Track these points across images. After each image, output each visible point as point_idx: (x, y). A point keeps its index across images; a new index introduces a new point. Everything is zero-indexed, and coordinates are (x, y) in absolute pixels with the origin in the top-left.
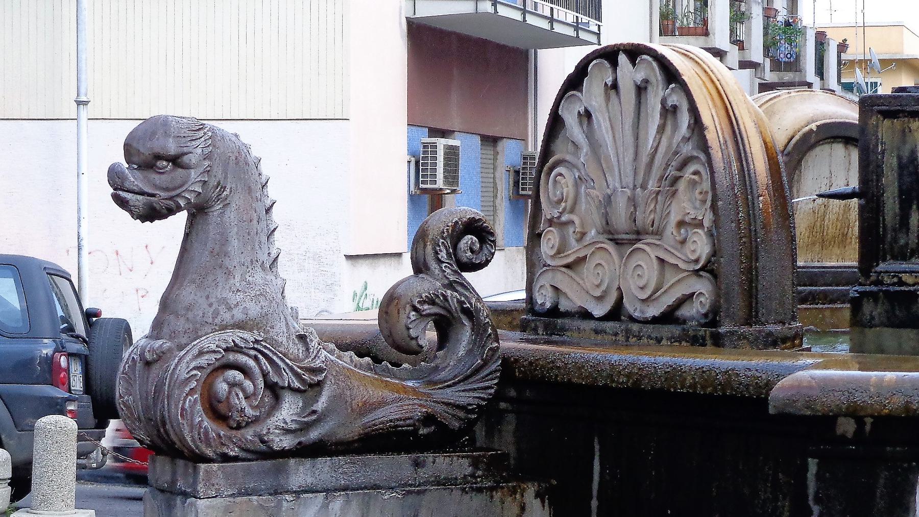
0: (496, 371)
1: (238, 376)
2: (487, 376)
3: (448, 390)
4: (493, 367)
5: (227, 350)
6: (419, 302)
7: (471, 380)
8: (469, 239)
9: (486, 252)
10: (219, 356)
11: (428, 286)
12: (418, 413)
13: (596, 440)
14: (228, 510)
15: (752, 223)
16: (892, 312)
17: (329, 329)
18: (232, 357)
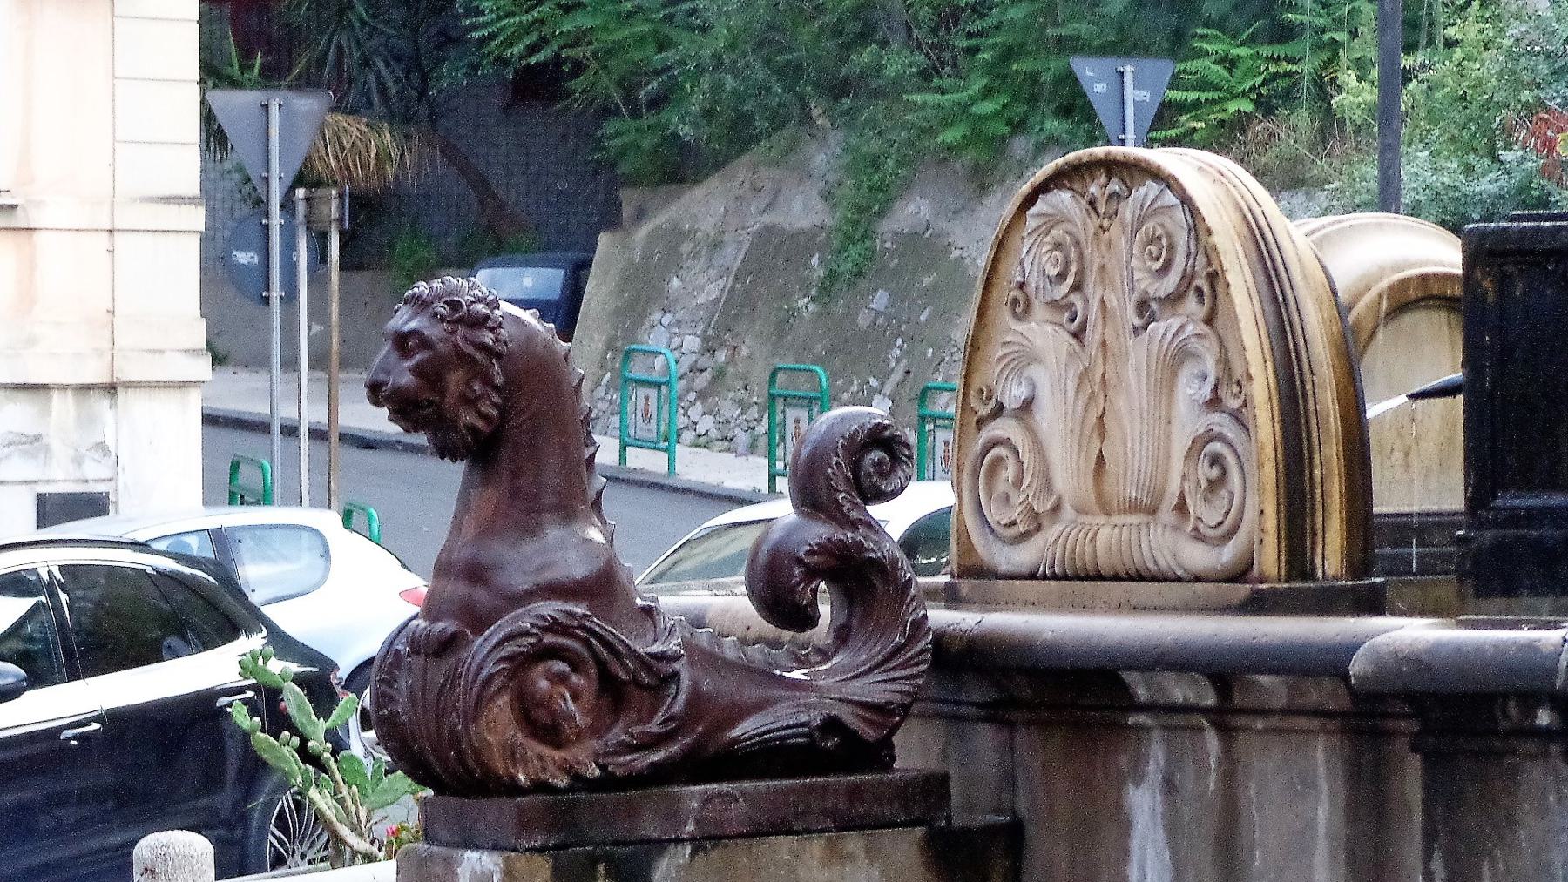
0: (923, 651)
1: (561, 666)
2: (911, 658)
3: (856, 683)
4: (922, 644)
5: (544, 629)
6: (807, 553)
7: (890, 665)
8: (876, 455)
9: (900, 474)
10: (533, 640)
11: (820, 531)
12: (816, 718)
13: (737, 732)
14: (689, 868)
15: (1316, 441)
16: (1495, 560)
17: (1048, 635)
18: (548, 639)
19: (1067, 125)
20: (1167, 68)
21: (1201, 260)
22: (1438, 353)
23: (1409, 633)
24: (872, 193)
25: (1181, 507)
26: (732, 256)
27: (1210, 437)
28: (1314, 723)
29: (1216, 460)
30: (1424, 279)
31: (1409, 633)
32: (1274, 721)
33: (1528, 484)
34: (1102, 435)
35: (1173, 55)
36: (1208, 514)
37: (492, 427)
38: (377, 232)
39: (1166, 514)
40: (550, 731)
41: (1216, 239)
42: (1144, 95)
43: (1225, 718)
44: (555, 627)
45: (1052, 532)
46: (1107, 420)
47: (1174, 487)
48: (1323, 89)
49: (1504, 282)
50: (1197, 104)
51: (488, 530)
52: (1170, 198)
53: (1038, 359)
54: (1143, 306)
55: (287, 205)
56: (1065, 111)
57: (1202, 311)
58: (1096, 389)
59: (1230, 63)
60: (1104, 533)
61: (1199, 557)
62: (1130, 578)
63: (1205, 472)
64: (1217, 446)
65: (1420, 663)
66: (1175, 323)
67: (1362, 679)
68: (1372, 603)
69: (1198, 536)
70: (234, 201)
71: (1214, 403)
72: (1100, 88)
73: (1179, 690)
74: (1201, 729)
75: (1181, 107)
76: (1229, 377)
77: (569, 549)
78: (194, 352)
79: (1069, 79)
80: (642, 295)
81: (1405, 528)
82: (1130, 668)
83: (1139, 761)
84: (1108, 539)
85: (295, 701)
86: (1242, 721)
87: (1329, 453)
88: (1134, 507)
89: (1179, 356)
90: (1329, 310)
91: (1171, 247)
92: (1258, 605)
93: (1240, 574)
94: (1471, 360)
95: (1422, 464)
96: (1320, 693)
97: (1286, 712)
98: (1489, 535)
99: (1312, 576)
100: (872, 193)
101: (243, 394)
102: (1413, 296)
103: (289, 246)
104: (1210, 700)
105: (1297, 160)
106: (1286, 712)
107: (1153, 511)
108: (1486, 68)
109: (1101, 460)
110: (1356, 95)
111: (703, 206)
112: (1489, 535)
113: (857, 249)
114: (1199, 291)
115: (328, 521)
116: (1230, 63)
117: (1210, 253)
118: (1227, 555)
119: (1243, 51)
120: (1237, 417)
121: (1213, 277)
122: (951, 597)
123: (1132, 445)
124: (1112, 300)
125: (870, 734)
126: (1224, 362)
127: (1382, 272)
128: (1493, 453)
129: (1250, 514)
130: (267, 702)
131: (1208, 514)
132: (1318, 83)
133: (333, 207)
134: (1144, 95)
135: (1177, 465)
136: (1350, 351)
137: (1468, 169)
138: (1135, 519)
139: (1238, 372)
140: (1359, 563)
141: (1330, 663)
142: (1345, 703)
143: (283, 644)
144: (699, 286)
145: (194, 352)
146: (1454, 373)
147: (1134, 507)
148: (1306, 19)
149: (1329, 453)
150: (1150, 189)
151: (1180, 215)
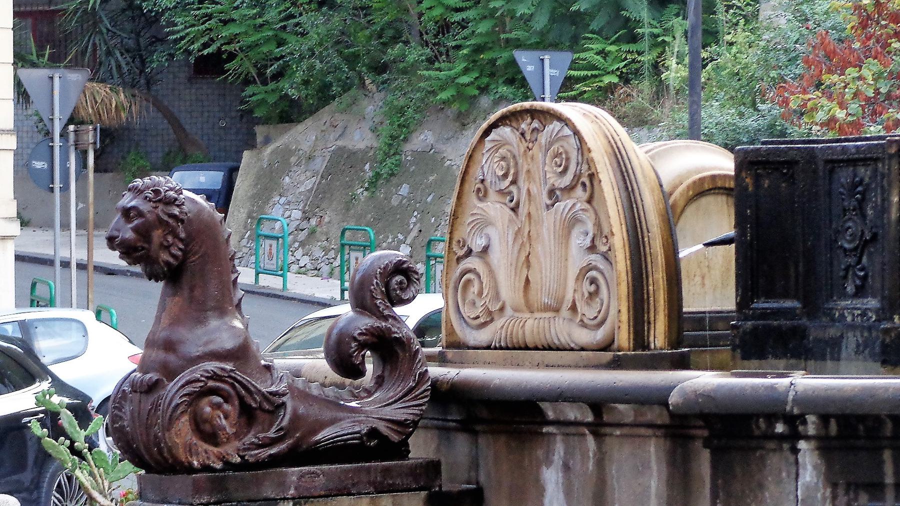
15: (650, 271)
20: (567, 57)
21: (585, 167)
22: (719, 218)
23: (703, 380)
24: (400, 129)
25: (574, 308)
26: (320, 164)
27: (590, 268)
28: (650, 432)
29: (593, 281)
30: (713, 177)
31: (703, 380)
32: (626, 430)
33: (770, 295)
34: (528, 267)
36: (589, 312)
37: (177, 261)
38: (114, 150)
39: (565, 312)
40: (212, 437)
42: (555, 72)
44: (215, 377)
45: (499, 323)
47: (569, 297)
48: (657, 68)
49: (757, 179)
50: (585, 78)
51: (175, 322)
53: (492, 223)
54: (552, 193)
55: (64, 135)
56: (510, 82)
58: (524, 241)
59: (603, 53)
60: (530, 323)
61: (584, 337)
64: (593, 273)
65: (708, 396)
66: (570, 203)
67: (676, 406)
68: (682, 363)
69: (583, 325)
70: (34, 134)
71: (592, 248)
72: (530, 68)
73: (572, 413)
74: (584, 435)
75: (579, 80)
76: (601, 232)
77: (223, 332)
79: (513, 63)
80: (268, 186)
81: (698, 320)
82: (543, 400)
83: (549, 454)
84: (532, 327)
85: (67, 420)
86: (608, 430)
88: (547, 308)
89: (573, 221)
91: (568, 159)
92: (617, 364)
93: (607, 346)
94: (740, 222)
95: (711, 285)
96: (654, 415)
100: (400, 129)
101: (38, 243)
102: (706, 188)
103: (65, 159)
104: (590, 418)
105: (644, 110)
107: (557, 310)
108: (750, 57)
109: (527, 281)
110: (675, 72)
111: (303, 136)
113: (390, 162)
114: (584, 184)
115: (88, 317)
117: (590, 162)
118: (600, 335)
120: (605, 256)
121: (592, 176)
122: (441, 359)
123: (545, 274)
124: (534, 190)
125: (395, 438)
126: (598, 225)
127: (690, 173)
129: (613, 312)
130: (51, 420)
133: (90, 136)
134: (555, 72)
135: (571, 283)
136: (670, 218)
137: (741, 115)
139: (606, 231)
140: (676, 340)
142: (666, 420)
143: (60, 387)
144: (302, 181)
146: (731, 233)
147: (547, 308)
150: (556, 125)
151: (573, 141)
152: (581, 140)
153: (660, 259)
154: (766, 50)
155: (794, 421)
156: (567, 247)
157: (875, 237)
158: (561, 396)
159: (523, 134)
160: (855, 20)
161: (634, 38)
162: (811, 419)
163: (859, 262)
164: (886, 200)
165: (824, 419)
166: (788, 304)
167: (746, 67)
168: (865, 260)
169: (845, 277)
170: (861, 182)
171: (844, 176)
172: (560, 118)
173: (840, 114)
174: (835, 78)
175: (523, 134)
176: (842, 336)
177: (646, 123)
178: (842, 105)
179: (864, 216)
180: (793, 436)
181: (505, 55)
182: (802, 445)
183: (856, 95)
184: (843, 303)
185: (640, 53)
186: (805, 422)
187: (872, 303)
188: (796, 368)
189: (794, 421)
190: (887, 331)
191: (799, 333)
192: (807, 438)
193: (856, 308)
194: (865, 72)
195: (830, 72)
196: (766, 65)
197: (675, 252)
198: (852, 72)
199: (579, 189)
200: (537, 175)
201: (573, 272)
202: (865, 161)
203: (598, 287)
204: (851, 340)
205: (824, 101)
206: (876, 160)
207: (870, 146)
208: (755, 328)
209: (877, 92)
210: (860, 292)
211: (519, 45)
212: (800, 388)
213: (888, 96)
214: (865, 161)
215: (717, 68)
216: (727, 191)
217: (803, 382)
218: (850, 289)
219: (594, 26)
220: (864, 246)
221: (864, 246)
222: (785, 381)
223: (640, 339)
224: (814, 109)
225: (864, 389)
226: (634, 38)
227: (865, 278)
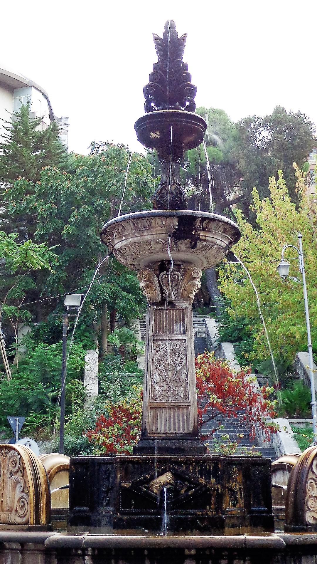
15: (41, 497)
19: (7, 428)
20: (24, 419)
21: (22, 465)
22: (64, 480)
23: (56, 536)
25: (16, 511)
28: (38, 552)
29: (23, 502)
30: (64, 465)
31: (56, 536)
32: (31, 552)
33: (80, 505)
34: (3, 497)
35: (26, 416)
36: (21, 512)
39: (14, 512)
41: (24, 461)
42: (20, 423)
43: (22, 551)
46: (4, 494)
47: (15, 507)
48: (52, 423)
49: (77, 469)
50: (30, 425)
52: (16, 454)
54: (11, 473)
56: (6, 426)
57: (21, 475)
59: (36, 417)
60: (2, 515)
61: (19, 520)
62: (6, 524)
63: (21, 504)
64: (23, 499)
65: (57, 542)
66: (16, 476)
67: (47, 545)
68: (50, 529)
69: (19, 516)
71: (23, 491)
72: (12, 422)
73: (14, 546)
74: (18, 553)
75: (28, 425)
76: (26, 486)
78: (170, 84)
79: (7, 420)
81: (59, 512)
82: (5, 542)
83: (6, 559)
86: (26, 552)
87: (43, 501)
88: (8, 510)
89: (17, 483)
90: (45, 474)
91: (16, 462)
92: (30, 529)
93: (27, 523)
94: (71, 482)
95: (61, 500)
96: (40, 547)
97: (33, 550)
98: (73, 515)
99: (40, 524)
102: (61, 469)
104: (20, 548)
105: (47, 435)
106: (33, 550)
107: (11, 511)
108: (81, 420)
109: (2, 501)
110: (57, 424)
112: (73, 515)
114: (21, 471)
116: (36, 417)
117: (23, 464)
118: (24, 520)
119: (39, 416)
120: (27, 494)
121: (24, 468)
124: (5, 472)
126: (25, 484)
127: (57, 464)
128: (74, 499)
129: (29, 512)
131: (21, 512)
132: (52, 422)
134: (20, 423)
135: (16, 503)
137: (77, 438)
138: (8, 513)
139: (27, 485)
140: (49, 520)
141: (41, 541)
142: (44, 549)
145: (170, 84)
146: (68, 484)
147: (8, 510)
148: (50, 410)
149: (43, 501)
150: (13, 451)
151: (18, 457)
152: (21, 456)
153: (44, 495)
154: (86, 418)
155: (84, 550)
156: (15, 490)
157: (112, 487)
158: (11, 540)
159: (2, 454)
160: (112, 411)
161: (45, 412)
162: (89, 549)
163: (107, 495)
164: (116, 476)
165: (93, 549)
166: (85, 508)
167: (80, 423)
168: (109, 495)
169: (103, 500)
170: (108, 470)
171: (103, 468)
172: (14, 449)
173: (107, 441)
174: (106, 429)
175: (2, 454)
176: (101, 520)
177: (48, 440)
178: (108, 438)
179: (109, 481)
180: (84, 555)
181: (5, 417)
182: (87, 557)
183: (112, 435)
184: (102, 508)
185: (47, 418)
186: (87, 550)
187: (111, 508)
188: (85, 531)
189: (84, 550)
190: (115, 518)
191: (88, 518)
192: (88, 555)
193: (106, 510)
194: (115, 428)
195: (104, 427)
196: (85, 422)
197: (49, 491)
198: (111, 428)
199: (20, 473)
200: (6, 467)
201: (17, 499)
202: (110, 464)
203: (24, 504)
204: (105, 520)
205: (102, 436)
206: (113, 463)
207: (112, 459)
208: (75, 516)
209: (118, 434)
210: (108, 505)
211: (9, 414)
212: (86, 539)
213: (122, 435)
214: (110, 464)
215: (71, 423)
216: (67, 470)
217: (87, 537)
218: (104, 504)
219: (34, 408)
220: (109, 490)
221: (109, 490)
222: (82, 537)
223: (37, 521)
224: (99, 439)
225: (106, 539)
226: (45, 412)
227: (109, 500)
